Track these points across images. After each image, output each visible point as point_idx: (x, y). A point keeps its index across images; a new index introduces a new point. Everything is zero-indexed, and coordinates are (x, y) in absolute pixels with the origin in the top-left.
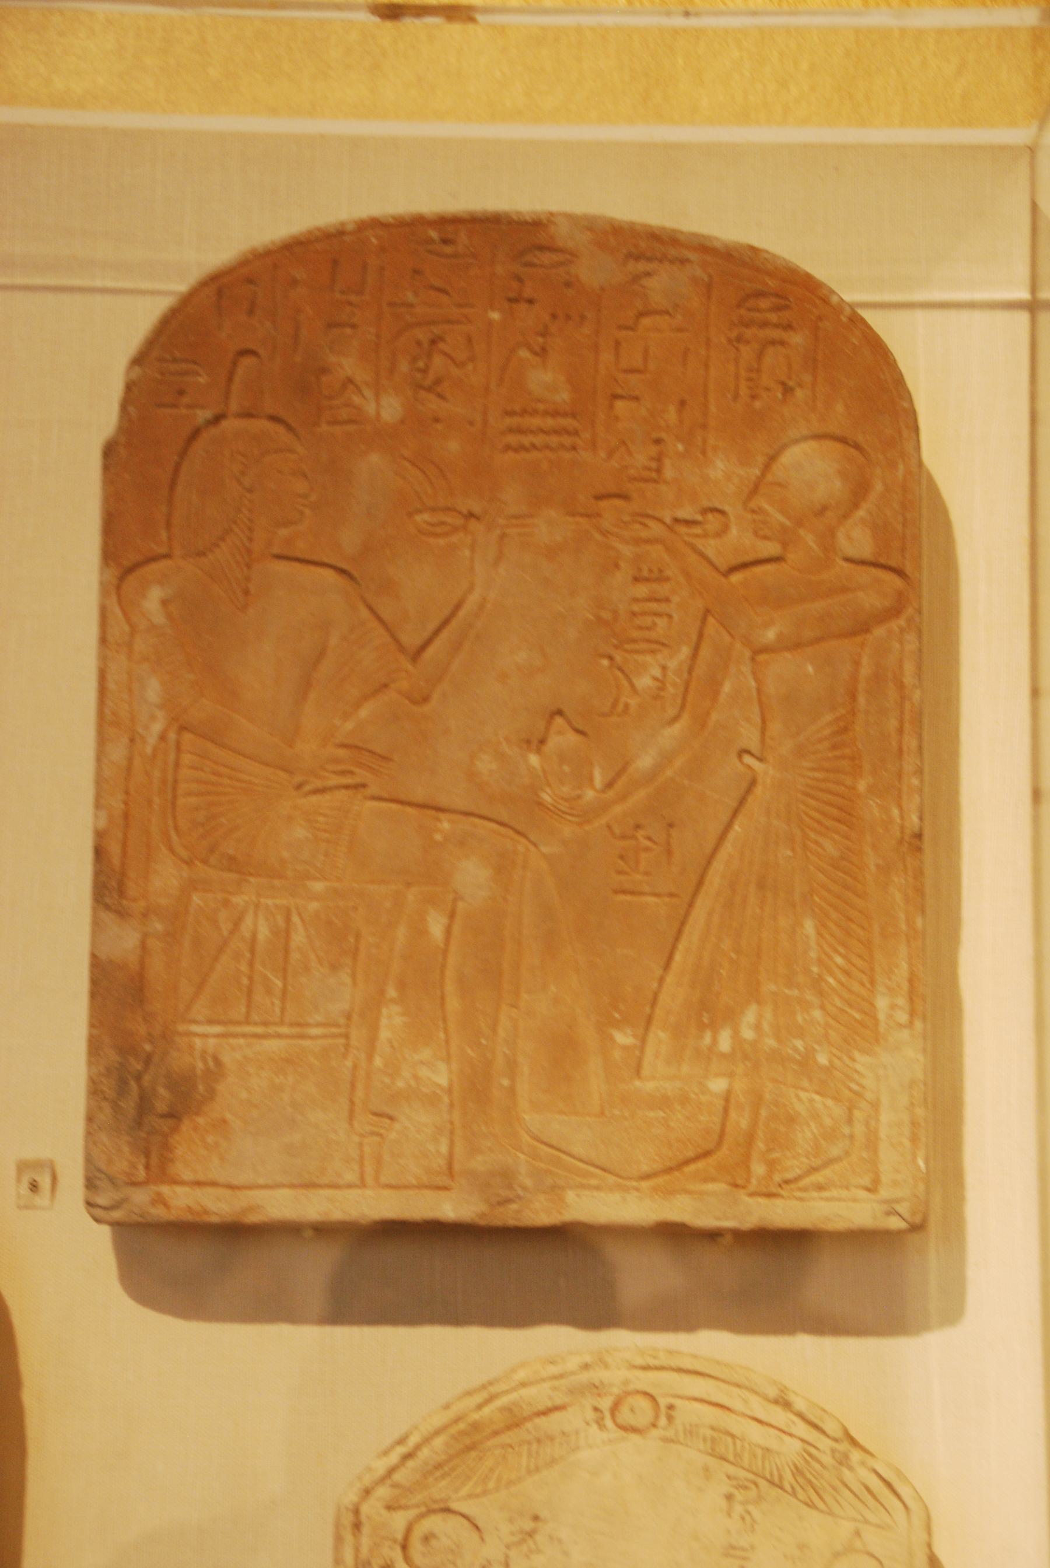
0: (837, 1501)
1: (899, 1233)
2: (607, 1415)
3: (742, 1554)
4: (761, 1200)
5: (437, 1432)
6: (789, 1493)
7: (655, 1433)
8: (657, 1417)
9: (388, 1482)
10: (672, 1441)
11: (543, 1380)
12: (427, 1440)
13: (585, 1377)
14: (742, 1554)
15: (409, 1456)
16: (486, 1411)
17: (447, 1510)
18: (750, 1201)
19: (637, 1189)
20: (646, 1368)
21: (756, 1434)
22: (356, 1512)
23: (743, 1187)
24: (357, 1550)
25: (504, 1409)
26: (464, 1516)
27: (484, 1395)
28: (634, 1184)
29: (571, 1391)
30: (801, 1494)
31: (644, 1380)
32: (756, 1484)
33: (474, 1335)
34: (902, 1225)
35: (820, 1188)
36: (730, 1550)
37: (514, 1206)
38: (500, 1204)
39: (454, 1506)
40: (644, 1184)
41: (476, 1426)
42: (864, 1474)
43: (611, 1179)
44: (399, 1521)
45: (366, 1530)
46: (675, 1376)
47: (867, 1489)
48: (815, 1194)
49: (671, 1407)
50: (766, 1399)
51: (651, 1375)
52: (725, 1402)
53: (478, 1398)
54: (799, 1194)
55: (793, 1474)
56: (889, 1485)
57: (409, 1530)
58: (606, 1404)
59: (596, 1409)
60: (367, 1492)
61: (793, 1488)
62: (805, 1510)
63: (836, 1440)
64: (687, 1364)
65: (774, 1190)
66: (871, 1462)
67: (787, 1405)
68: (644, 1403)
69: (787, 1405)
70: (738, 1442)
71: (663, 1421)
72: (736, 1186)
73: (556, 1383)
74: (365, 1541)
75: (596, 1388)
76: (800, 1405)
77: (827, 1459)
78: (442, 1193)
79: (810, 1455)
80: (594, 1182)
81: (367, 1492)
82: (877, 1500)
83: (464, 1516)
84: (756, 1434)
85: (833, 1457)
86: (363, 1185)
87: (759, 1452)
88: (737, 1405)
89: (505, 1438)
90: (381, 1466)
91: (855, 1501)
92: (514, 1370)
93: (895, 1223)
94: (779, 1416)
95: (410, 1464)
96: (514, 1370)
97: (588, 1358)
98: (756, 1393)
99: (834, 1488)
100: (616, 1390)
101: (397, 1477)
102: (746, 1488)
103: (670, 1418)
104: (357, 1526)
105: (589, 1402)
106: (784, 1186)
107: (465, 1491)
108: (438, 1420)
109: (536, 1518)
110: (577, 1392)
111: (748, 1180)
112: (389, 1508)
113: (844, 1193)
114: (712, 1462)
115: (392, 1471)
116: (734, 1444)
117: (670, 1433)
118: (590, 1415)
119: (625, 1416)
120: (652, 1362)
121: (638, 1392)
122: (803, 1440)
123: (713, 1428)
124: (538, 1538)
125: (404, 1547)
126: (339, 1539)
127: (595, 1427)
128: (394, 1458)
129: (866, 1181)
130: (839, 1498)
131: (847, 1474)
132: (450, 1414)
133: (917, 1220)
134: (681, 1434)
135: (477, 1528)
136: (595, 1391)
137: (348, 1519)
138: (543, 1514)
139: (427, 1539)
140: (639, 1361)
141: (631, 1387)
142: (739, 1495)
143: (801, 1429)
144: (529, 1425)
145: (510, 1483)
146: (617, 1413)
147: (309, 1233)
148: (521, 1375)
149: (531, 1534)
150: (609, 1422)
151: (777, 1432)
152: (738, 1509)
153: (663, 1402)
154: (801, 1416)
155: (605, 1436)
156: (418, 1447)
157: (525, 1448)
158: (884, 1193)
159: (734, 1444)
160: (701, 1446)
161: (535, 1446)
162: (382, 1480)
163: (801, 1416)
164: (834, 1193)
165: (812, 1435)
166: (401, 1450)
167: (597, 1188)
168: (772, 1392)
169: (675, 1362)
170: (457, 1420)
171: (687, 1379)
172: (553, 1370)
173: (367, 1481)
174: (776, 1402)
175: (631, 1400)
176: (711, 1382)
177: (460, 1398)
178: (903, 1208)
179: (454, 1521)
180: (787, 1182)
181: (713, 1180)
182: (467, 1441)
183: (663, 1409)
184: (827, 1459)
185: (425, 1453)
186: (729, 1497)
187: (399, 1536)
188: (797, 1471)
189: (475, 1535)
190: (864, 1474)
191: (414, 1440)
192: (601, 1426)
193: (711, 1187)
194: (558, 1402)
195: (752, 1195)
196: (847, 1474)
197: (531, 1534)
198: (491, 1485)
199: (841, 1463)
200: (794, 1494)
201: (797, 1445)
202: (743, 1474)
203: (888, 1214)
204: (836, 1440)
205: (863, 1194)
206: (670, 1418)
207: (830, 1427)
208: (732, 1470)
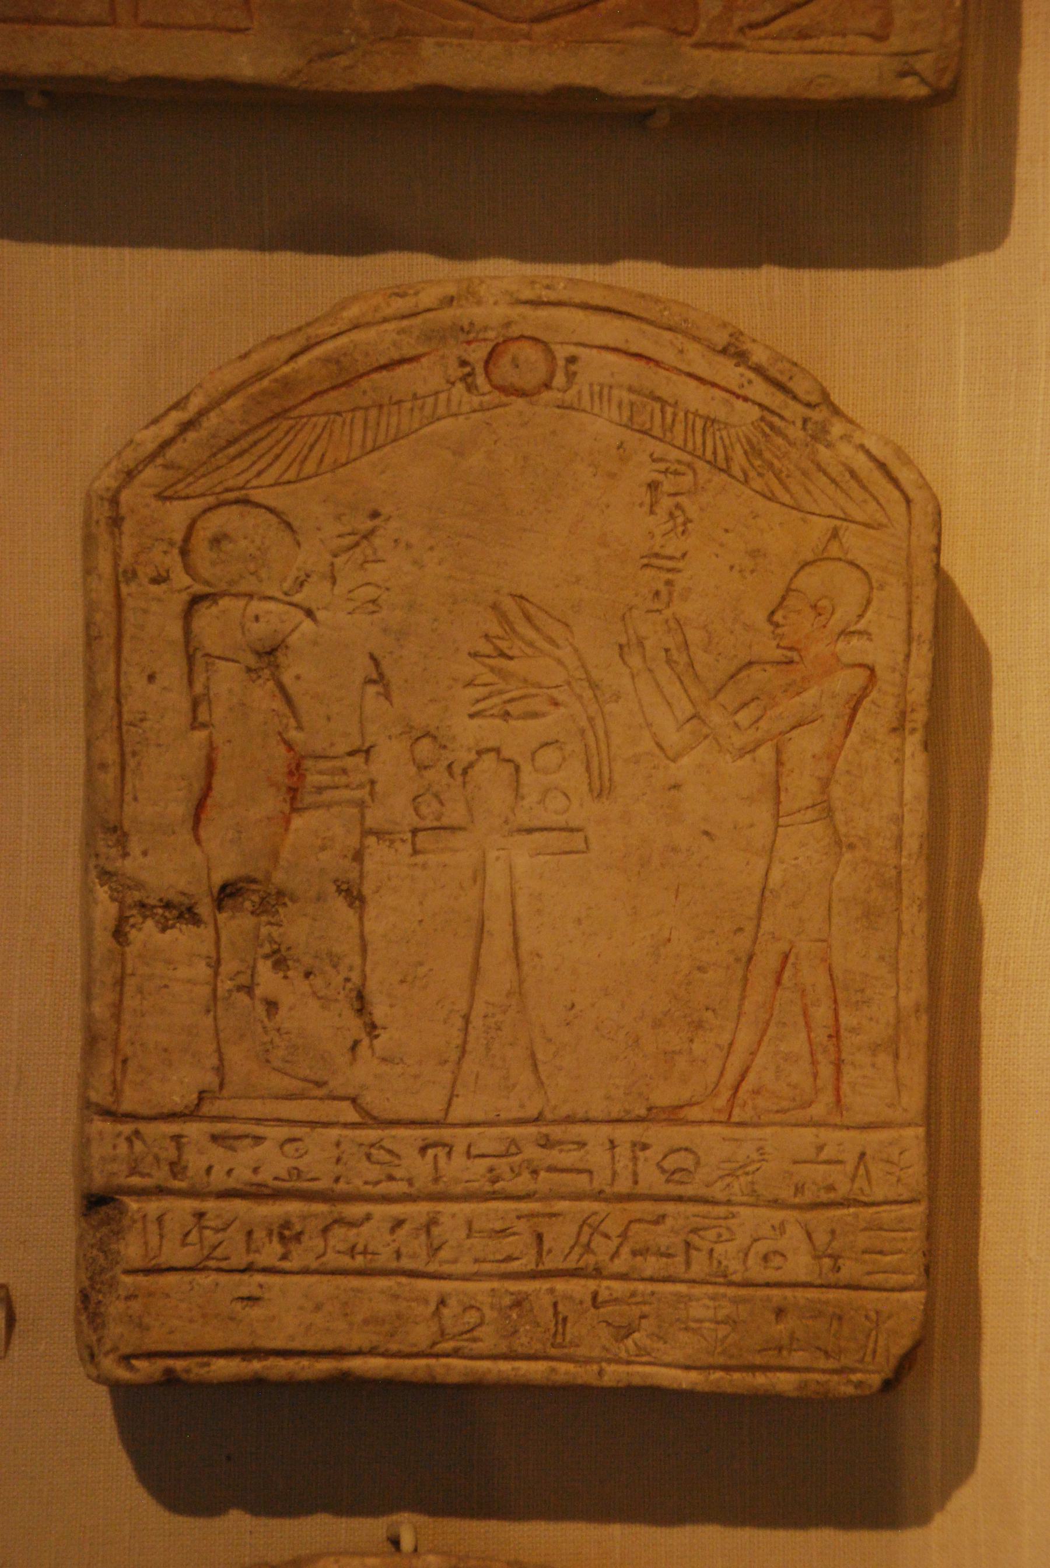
0: (809, 492)
1: (917, 104)
2: (479, 370)
3: (670, 564)
4: (716, 55)
5: (230, 393)
6: (738, 480)
7: (546, 396)
8: (552, 375)
9: (159, 461)
10: (571, 407)
11: (385, 320)
12: (216, 403)
13: (447, 315)
14: (670, 564)
15: (186, 427)
16: (303, 360)
17: (246, 502)
18: (696, 53)
19: (528, 36)
20: (537, 303)
21: (693, 396)
22: (114, 501)
23: (688, 34)
24: (116, 556)
25: (327, 360)
26: (270, 510)
27: (301, 340)
28: (524, 27)
29: (427, 336)
30: (757, 484)
31: (536, 319)
32: (689, 465)
33: (156, 69)
34: (923, 91)
35: (803, 35)
36: (652, 559)
37: (344, 61)
38: (321, 56)
39: (257, 495)
40: (540, 29)
41: (287, 385)
42: (846, 450)
43: (490, 21)
44: (177, 515)
45: (128, 526)
46: (580, 314)
47: (853, 474)
48: (796, 45)
49: (572, 360)
50: (711, 348)
51: (543, 313)
52: (650, 350)
53: (290, 346)
54: (768, 44)
55: (746, 453)
56: (882, 466)
57: (191, 528)
58: (478, 354)
59: (464, 363)
60: (130, 475)
61: (746, 475)
62: (760, 503)
63: (808, 405)
64: (597, 299)
65: (730, 38)
66: (858, 437)
67: (741, 357)
68: (529, 353)
69: (741, 357)
70: (669, 410)
71: (559, 380)
72: (676, 32)
73: (405, 323)
74: (128, 545)
75: (466, 332)
76: (759, 356)
77: (795, 433)
78: (235, 38)
79: (772, 427)
80: (463, 24)
81: (130, 475)
82: (864, 487)
83: (270, 510)
84: (693, 396)
85: (804, 428)
86: (114, 23)
87: (699, 424)
88: (669, 356)
89: (331, 401)
90: (150, 438)
91: (831, 489)
92: (343, 305)
93: (912, 89)
94: (730, 373)
95: (191, 436)
96: (343, 305)
97: (451, 290)
98: (696, 339)
99: (804, 473)
100: (875, 590)
101: (171, 453)
102: (676, 473)
103: (571, 376)
104: (116, 521)
105: (454, 351)
106: (747, 30)
107: (270, 477)
108: (231, 376)
109: (375, 515)
110: (437, 336)
111: (696, 25)
112: (160, 497)
113: (838, 42)
114: (632, 439)
115: (166, 444)
116: (663, 412)
117: (570, 396)
118: (456, 372)
119: (504, 371)
120: (547, 295)
121: (522, 337)
122: (760, 405)
123: (631, 389)
124: (377, 541)
125: (184, 552)
126: (89, 541)
127: (460, 386)
128: (168, 428)
129: (871, 23)
130: (811, 487)
131: (823, 451)
132: (251, 365)
133: (945, 82)
134: (586, 397)
135: (289, 525)
136: (462, 337)
137: (102, 512)
138: (385, 511)
139: (216, 541)
140: (527, 294)
141: (515, 331)
142: (668, 485)
143: (760, 390)
144: (364, 383)
145: (337, 466)
146: (491, 366)
147: (36, 100)
148: (353, 312)
149: (367, 536)
150: (481, 380)
151: (727, 396)
152: (666, 503)
153: (562, 353)
154: (758, 370)
155: (476, 400)
156: (202, 413)
157: (359, 414)
158: (896, 43)
159: (663, 412)
160: (615, 414)
161: (373, 413)
162: (152, 457)
163: (758, 370)
164: (822, 42)
165: (775, 399)
166: (177, 417)
167: (470, 34)
168: (721, 338)
169: (579, 297)
170: (260, 375)
171: (596, 319)
172: (400, 305)
173: (130, 458)
174: (724, 351)
175: (513, 348)
176: (629, 323)
177: (265, 343)
178: (924, 64)
179: (255, 518)
180: (752, 26)
181: (643, 23)
182: (275, 406)
183: (561, 363)
184: (795, 433)
185: (213, 420)
186: (653, 486)
187: (178, 537)
188: (753, 451)
189: (288, 539)
190: (846, 450)
191: (196, 403)
192: (471, 388)
193: (638, 33)
194: (408, 352)
195: (697, 46)
196: (823, 451)
197: (367, 536)
198: (310, 467)
199: (814, 438)
200: (746, 482)
201: (756, 412)
202: (675, 454)
203: (903, 74)
204: (808, 405)
205: (864, 43)
206: (571, 376)
207: (799, 387)
208: (659, 449)
